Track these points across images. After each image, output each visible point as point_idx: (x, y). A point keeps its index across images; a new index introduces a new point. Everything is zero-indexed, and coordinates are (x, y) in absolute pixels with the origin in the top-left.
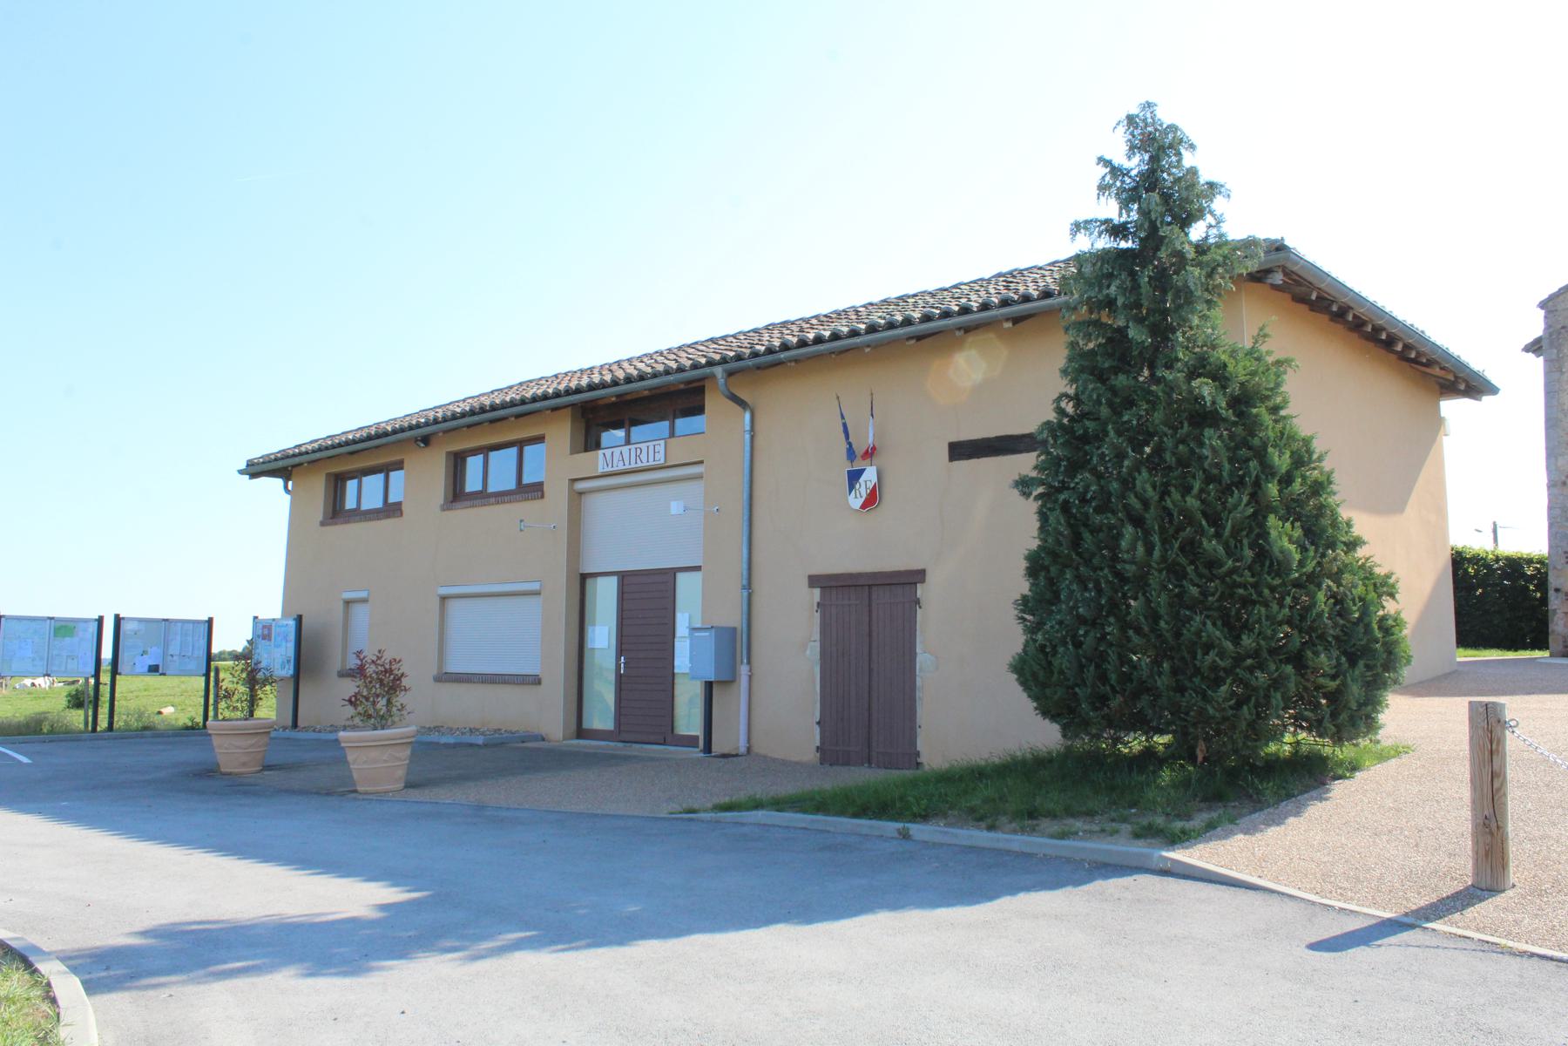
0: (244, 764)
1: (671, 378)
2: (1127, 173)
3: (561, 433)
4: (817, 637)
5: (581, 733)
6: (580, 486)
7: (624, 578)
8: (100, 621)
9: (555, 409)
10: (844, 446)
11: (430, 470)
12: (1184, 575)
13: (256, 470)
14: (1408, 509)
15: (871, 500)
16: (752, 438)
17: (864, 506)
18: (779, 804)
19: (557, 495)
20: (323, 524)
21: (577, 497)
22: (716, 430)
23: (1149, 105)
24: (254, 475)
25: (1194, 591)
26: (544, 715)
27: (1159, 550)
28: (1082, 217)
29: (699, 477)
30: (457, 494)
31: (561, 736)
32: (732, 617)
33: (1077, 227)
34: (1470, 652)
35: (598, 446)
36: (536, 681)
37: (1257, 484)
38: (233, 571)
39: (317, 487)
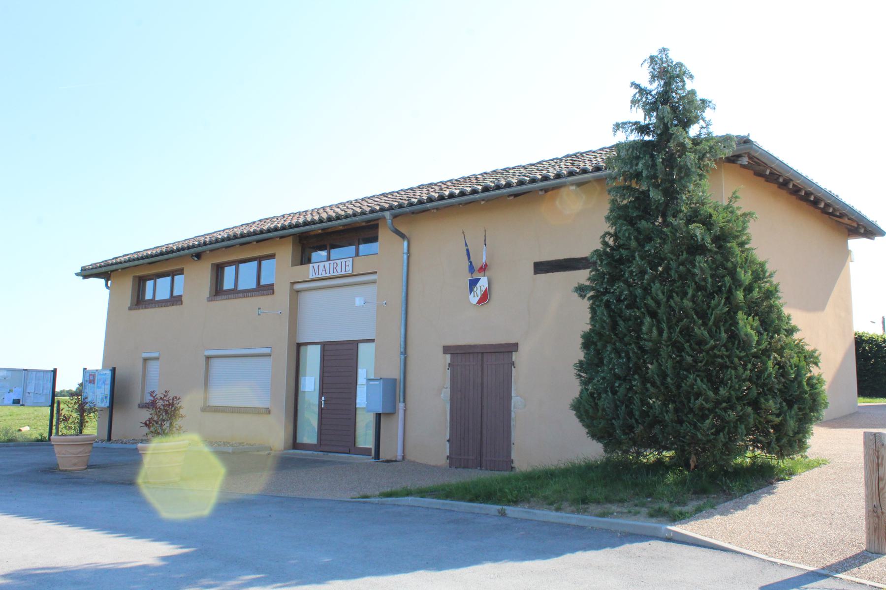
0: (75, 465)
2: (649, 93)
3: (286, 253)
4: (448, 385)
7: (325, 346)
13: (87, 273)
15: (484, 298)
16: (408, 258)
17: (479, 302)
20: (130, 309)
21: (295, 294)
22: (386, 250)
24: (86, 277)
30: (218, 291)
33: (617, 126)
35: (309, 261)
39: (127, 286)
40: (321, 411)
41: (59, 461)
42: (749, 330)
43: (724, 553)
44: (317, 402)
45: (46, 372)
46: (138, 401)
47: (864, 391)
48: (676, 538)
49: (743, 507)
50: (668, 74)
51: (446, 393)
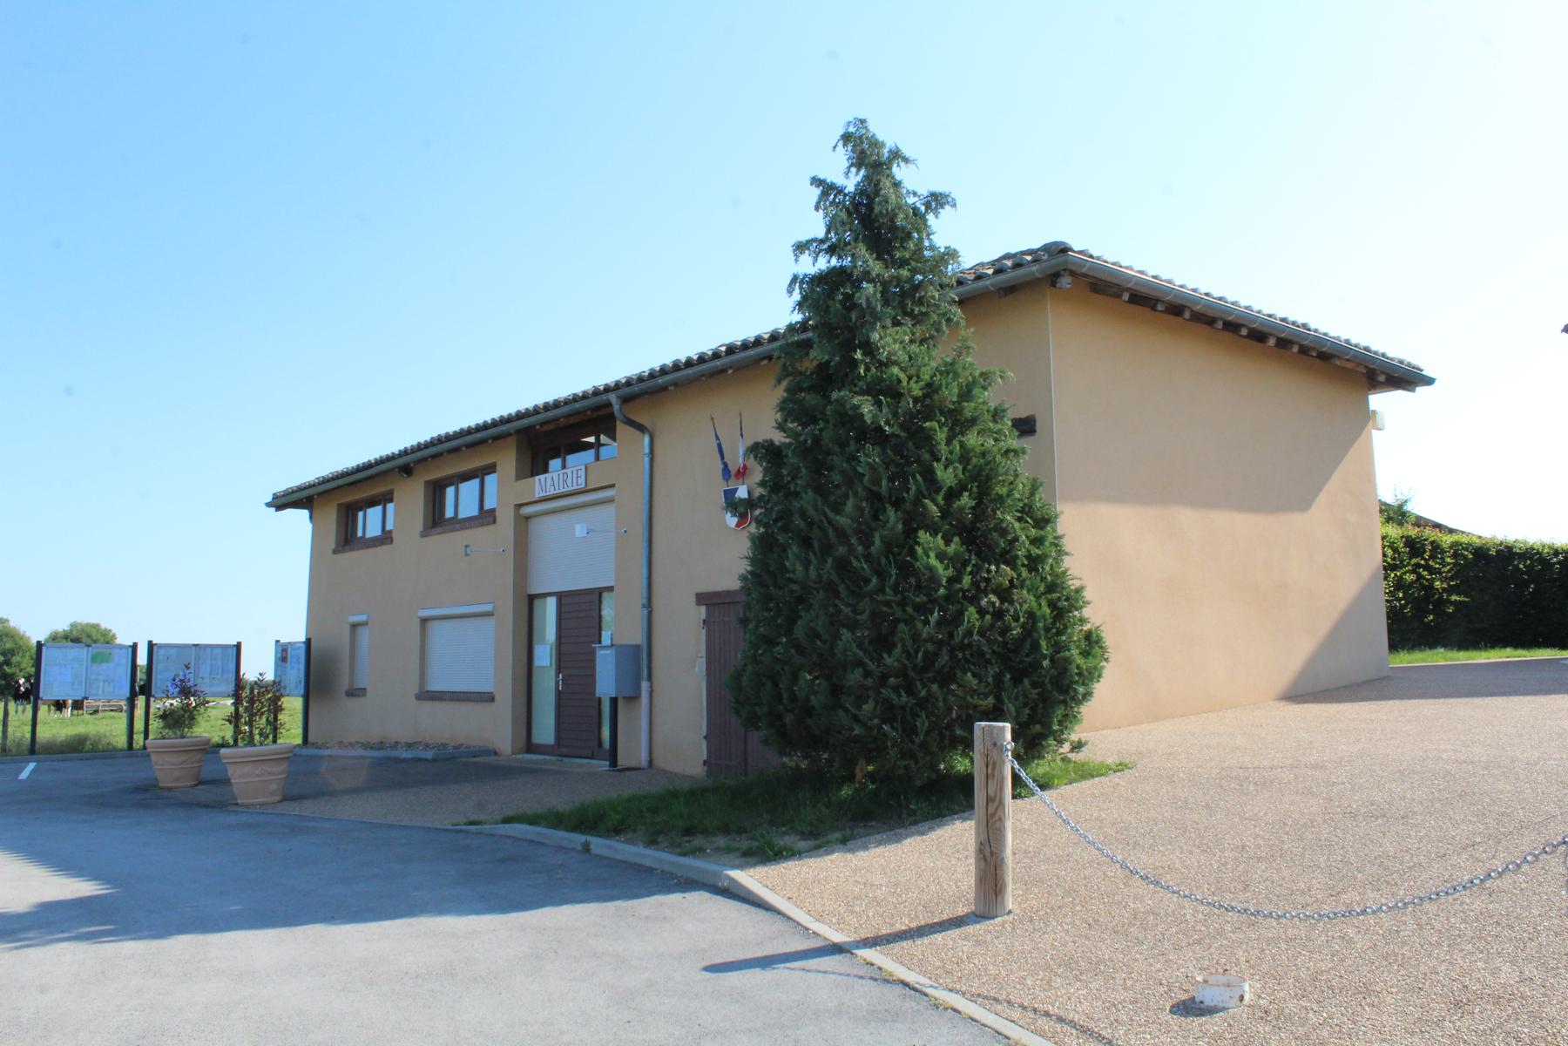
0: (177, 779)
1: (577, 405)
2: (840, 191)
3: (507, 461)
4: (703, 653)
5: (530, 747)
6: (526, 511)
7: (561, 597)
8: (134, 647)
9: (496, 438)
10: (721, 466)
11: (408, 505)
12: (837, 594)
13: (283, 502)
14: (1314, 508)
16: (652, 460)
18: (533, 820)
19: (506, 519)
20: (335, 552)
21: (523, 523)
22: (620, 453)
23: (863, 121)
24: (280, 507)
25: (847, 610)
26: (494, 729)
27: (856, 562)
28: (804, 238)
29: (610, 500)
30: (436, 519)
31: (510, 752)
32: (636, 637)
33: (800, 248)
34: (1520, 652)
35: (546, 471)
36: (489, 698)
37: (917, 501)
38: (251, 596)
39: (331, 516)
40: (559, 694)
41: (157, 774)
42: (933, 561)
43: (762, 912)
44: (553, 684)
45: (225, 647)
46: (345, 686)
47: (1394, 646)
48: (734, 890)
49: (899, 839)
50: (868, 154)
51: (701, 665)
